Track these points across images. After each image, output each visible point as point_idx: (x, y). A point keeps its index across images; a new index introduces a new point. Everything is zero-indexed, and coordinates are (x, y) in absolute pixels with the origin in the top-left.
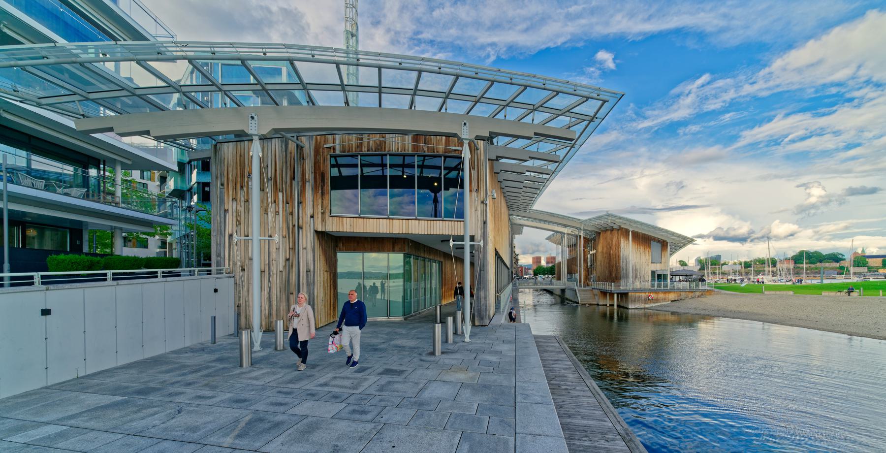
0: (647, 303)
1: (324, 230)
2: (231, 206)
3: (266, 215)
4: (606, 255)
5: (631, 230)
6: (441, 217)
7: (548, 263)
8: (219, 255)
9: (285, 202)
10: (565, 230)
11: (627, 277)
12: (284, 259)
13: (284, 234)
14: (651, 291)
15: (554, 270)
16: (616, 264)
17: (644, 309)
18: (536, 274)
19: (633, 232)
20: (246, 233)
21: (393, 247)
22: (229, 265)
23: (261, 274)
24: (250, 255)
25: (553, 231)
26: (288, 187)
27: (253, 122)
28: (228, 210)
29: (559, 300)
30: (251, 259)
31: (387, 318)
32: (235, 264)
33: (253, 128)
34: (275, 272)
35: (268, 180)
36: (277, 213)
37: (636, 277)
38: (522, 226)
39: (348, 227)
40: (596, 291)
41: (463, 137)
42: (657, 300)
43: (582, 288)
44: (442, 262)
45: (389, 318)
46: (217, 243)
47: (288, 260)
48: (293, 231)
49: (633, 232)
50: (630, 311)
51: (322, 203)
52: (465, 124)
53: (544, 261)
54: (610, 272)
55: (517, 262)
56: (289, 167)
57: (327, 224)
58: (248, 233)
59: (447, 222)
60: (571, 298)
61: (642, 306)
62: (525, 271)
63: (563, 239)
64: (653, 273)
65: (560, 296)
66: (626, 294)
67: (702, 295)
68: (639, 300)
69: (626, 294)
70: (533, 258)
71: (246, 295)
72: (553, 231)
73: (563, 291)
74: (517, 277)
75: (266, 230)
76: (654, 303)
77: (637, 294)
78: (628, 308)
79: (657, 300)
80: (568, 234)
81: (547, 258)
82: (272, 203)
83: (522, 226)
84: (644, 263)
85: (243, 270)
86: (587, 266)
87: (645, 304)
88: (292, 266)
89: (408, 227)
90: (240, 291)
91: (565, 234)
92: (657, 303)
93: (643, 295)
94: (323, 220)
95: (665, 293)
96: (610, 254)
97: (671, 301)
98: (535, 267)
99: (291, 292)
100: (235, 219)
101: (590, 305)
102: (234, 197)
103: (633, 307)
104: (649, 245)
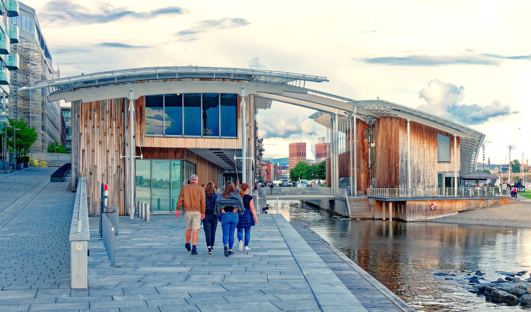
0: (429, 215)
2: (83, 130)
3: (105, 136)
4: (386, 151)
5: (409, 120)
6: (219, 136)
7: (318, 155)
8: (76, 164)
9: (117, 128)
10: (336, 111)
11: (406, 182)
12: (117, 166)
13: (117, 149)
14: (434, 199)
15: (325, 171)
16: (395, 166)
17: (426, 221)
18: (294, 178)
19: (411, 122)
20: (93, 149)
21: (175, 155)
22: (83, 170)
23: (102, 177)
24: (95, 164)
26: (119, 118)
27: (131, 92)
28: (82, 133)
29: (326, 215)
30: (96, 167)
31: (170, 211)
32: (86, 170)
34: (110, 175)
35: (107, 112)
36: (112, 135)
37: (419, 181)
38: (271, 100)
39: (158, 144)
40: (372, 200)
41: (242, 95)
42: (441, 211)
43: (356, 197)
44: (196, 165)
45: (171, 212)
46: (75, 156)
47: (119, 167)
48: (123, 147)
49: (411, 122)
50: (408, 224)
51: (141, 127)
52: (243, 88)
53: (312, 151)
54: (390, 174)
55: (261, 155)
56: (120, 104)
57: (144, 142)
58: (94, 148)
59: (223, 140)
60: (341, 212)
61: (423, 218)
62: (275, 172)
63: (334, 122)
64: (440, 176)
65: (328, 211)
66: (404, 203)
67: (496, 203)
68: (419, 210)
69: (404, 203)
70: (291, 146)
71: (93, 191)
73: (332, 202)
74: (260, 184)
75: (105, 147)
76: (438, 214)
77: (417, 203)
78: (405, 221)
79: (441, 211)
80: (339, 115)
81: (318, 147)
82: (109, 128)
83: (271, 100)
84: (428, 162)
85: (91, 174)
86: (368, 164)
87: (427, 215)
88: (122, 171)
89: (197, 144)
90: (89, 188)
91: (336, 115)
92: (441, 214)
93: (424, 203)
94: (141, 139)
95: (451, 201)
96: (389, 150)
97: (459, 212)
98: (295, 161)
99: (121, 189)
100: (86, 140)
101: (364, 219)
102: (85, 125)
103: (412, 220)
104: (434, 139)
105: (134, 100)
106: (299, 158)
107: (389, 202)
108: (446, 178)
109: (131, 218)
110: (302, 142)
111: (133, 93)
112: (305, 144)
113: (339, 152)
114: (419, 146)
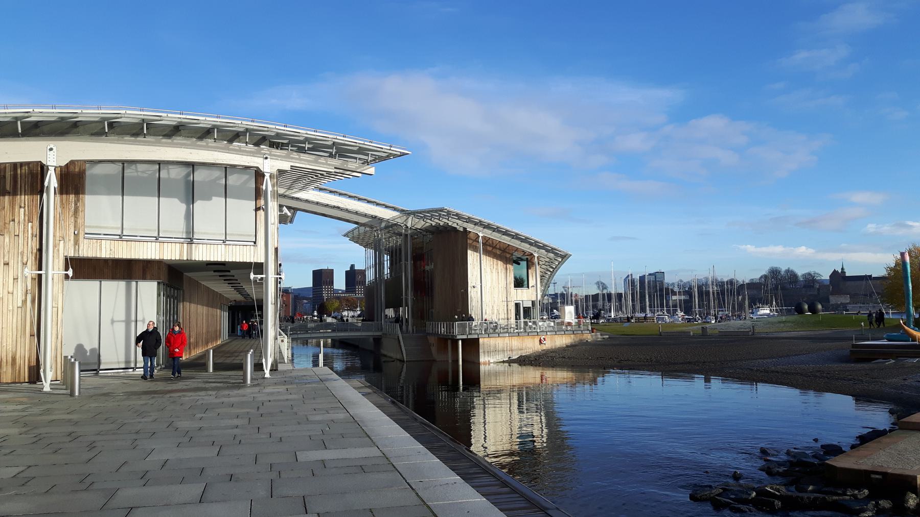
1: (77, 255)
5: (481, 235)
25: (356, 223)
33: (51, 159)
51: (76, 221)
64: (517, 306)
72: (356, 223)
94: (76, 242)
105: (56, 167)
106: (328, 287)
107: (459, 339)
108: (524, 308)
109: (45, 390)
110: (329, 268)
111: (55, 154)
112: (333, 270)
113: (386, 276)
114: (492, 268)
